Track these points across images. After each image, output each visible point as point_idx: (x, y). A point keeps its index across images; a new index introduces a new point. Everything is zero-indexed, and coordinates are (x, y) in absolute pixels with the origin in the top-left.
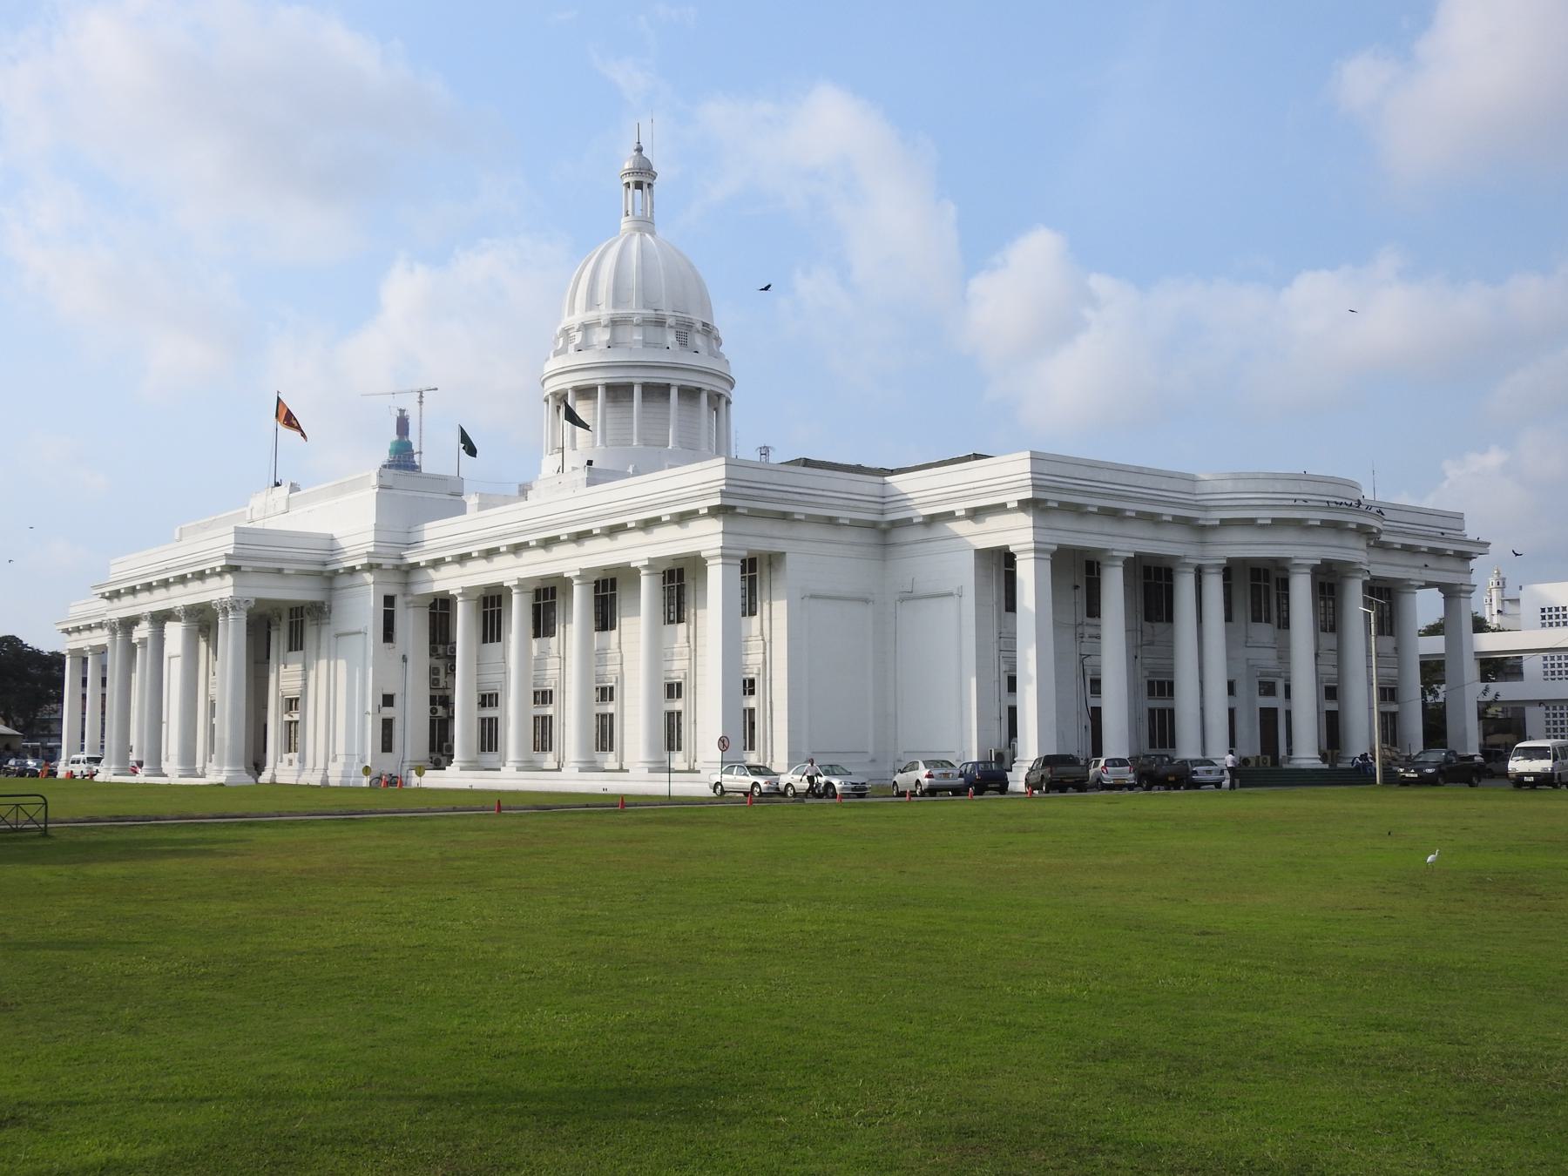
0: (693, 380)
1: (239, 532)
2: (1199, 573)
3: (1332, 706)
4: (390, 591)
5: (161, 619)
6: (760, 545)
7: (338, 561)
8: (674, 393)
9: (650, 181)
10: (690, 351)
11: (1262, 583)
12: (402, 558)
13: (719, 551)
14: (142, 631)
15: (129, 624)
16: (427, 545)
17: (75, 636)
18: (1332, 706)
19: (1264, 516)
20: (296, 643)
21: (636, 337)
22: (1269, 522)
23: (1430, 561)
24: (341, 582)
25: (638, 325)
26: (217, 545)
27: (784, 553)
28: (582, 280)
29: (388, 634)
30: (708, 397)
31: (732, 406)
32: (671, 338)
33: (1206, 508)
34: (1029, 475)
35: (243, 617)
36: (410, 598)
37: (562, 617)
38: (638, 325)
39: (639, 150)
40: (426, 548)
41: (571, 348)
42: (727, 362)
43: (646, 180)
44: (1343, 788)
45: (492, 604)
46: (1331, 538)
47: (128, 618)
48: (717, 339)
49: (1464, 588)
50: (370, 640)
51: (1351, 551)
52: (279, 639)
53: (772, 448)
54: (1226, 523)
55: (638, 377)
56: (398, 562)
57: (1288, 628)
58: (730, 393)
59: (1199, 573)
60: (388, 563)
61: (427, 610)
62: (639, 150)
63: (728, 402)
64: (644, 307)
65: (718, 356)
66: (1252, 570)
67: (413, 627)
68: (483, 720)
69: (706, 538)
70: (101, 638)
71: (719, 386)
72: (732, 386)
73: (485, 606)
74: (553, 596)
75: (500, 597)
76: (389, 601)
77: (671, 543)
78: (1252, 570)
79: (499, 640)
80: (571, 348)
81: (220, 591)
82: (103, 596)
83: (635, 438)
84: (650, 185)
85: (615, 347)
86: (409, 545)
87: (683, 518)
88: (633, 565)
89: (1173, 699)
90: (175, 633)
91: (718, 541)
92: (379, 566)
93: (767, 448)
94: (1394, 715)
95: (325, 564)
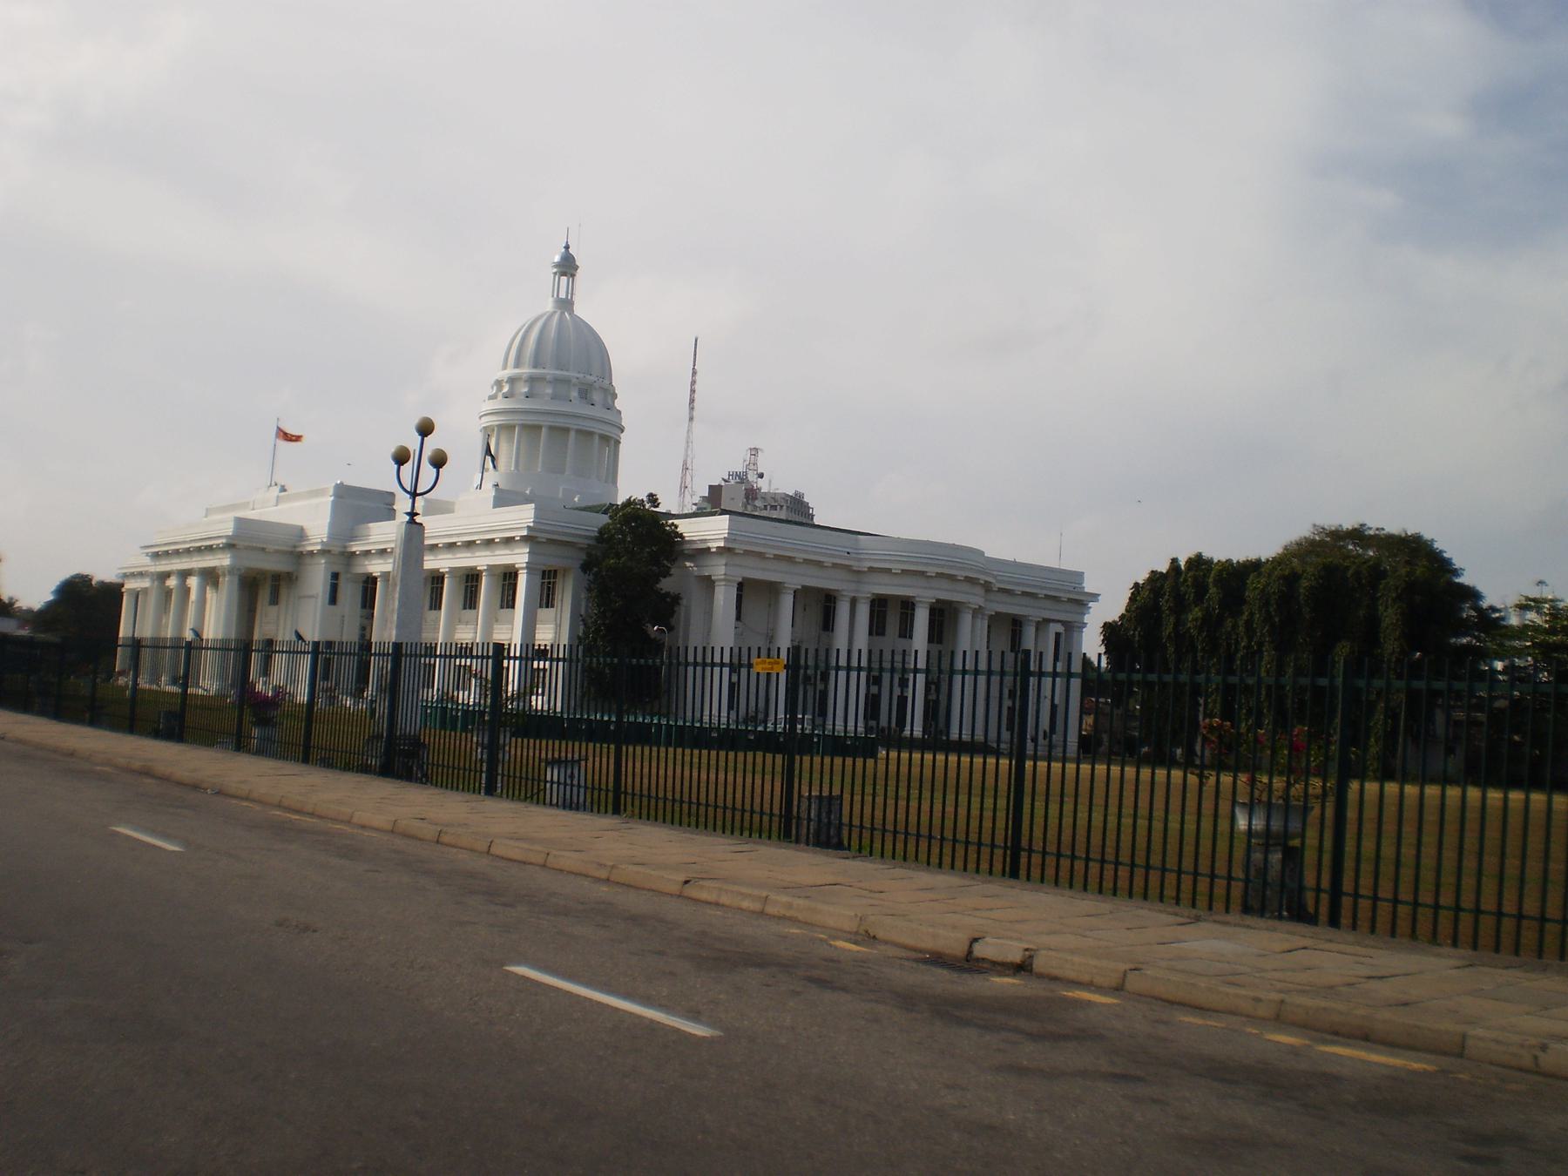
1: (240, 522)
2: (854, 602)
4: (336, 569)
5: (185, 574)
7: (304, 546)
10: (588, 403)
11: (909, 612)
12: (345, 547)
13: (525, 565)
14: (172, 582)
15: (165, 576)
16: (373, 539)
17: (767, 652)
19: (896, 567)
20: (275, 601)
22: (900, 572)
23: (1048, 604)
24: (308, 560)
25: (550, 382)
26: (224, 527)
28: (514, 345)
29: (333, 599)
32: (574, 394)
33: (860, 560)
34: (727, 531)
35: (236, 580)
36: (349, 575)
37: (560, 591)
38: (550, 382)
39: (567, 247)
40: (370, 541)
41: (500, 395)
42: (620, 412)
45: (471, 579)
46: (945, 584)
47: (163, 572)
49: (1076, 624)
50: (319, 604)
52: (264, 595)
53: (761, 450)
54: (871, 569)
55: (546, 421)
56: (342, 550)
57: (911, 637)
59: (854, 602)
60: (336, 550)
61: (361, 585)
62: (567, 247)
64: (557, 369)
65: (610, 407)
66: (902, 602)
67: (350, 594)
69: (519, 557)
70: (145, 583)
72: (622, 431)
73: (505, 580)
74: (555, 577)
75: (478, 575)
76: (335, 576)
77: (503, 557)
78: (902, 602)
79: (475, 608)
80: (500, 395)
81: (223, 561)
82: (147, 554)
83: (540, 465)
85: (532, 397)
86: (353, 538)
87: (508, 541)
88: (441, 571)
90: (193, 582)
91: (525, 558)
92: (329, 551)
93: (756, 449)
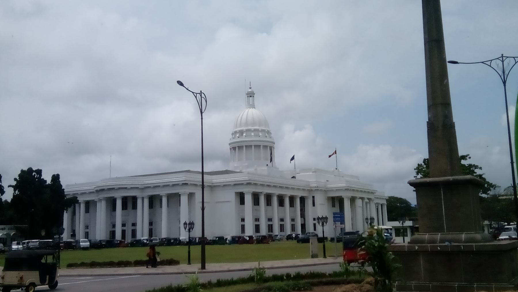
0: (266, 144)
2: (143, 199)
3: (293, 223)
6: (192, 191)
8: (262, 147)
9: (253, 95)
18: (293, 223)
21: (252, 134)
27: (195, 193)
30: (270, 148)
31: (275, 149)
41: (237, 137)
43: (252, 95)
44: (121, 235)
48: (271, 133)
51: (258, 190)
58: (274, 146)
59: (143, 199)
63: (274, 148)
68: (86, 232)
71: (271, 145)
72: (274, 144)
80: (237, 137)
84: (253, 96)
89: (122, 222)
94: (272, 225)
95: (325, 186)
